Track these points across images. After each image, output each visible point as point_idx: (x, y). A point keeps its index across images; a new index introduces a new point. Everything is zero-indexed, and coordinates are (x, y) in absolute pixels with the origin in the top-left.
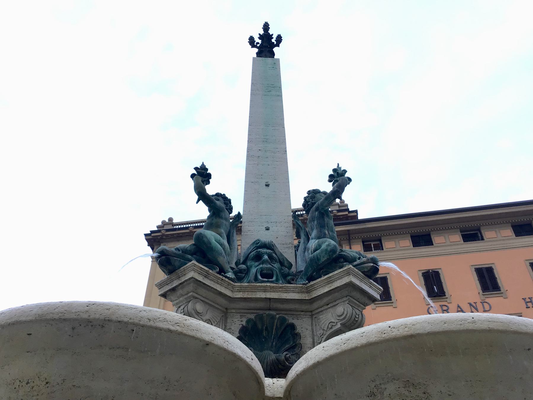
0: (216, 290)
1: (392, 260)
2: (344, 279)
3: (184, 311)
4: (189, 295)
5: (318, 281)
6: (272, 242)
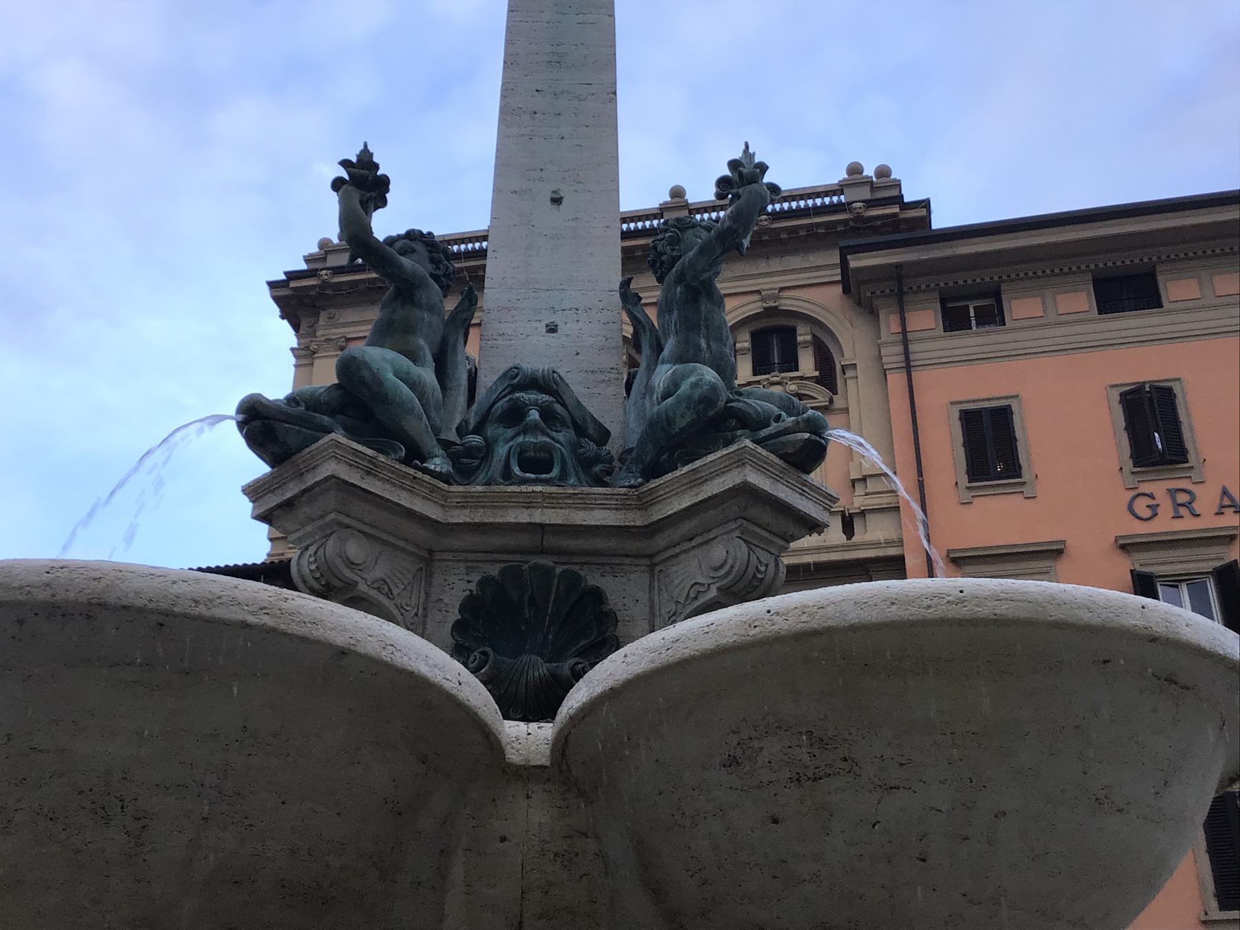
0: (399, 505)
3: (316, 560)
4: (328, 519)
5: (665, 480)
6: (554, 372)
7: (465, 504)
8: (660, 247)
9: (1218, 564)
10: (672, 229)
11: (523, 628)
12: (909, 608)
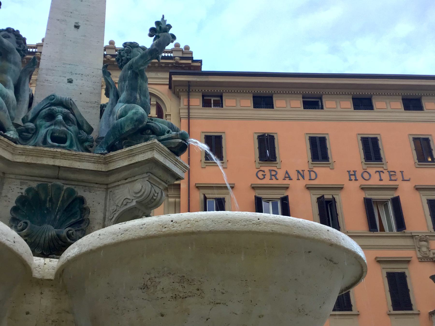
1: (232, 119)
2: (146, 154)
5: (118, 152)
6: (71, 100)
7: (23, 154)
8: (122, 54)
9: (282, 196)
10: (128, 46)
11: (45, 212)
12: (237, 225)
